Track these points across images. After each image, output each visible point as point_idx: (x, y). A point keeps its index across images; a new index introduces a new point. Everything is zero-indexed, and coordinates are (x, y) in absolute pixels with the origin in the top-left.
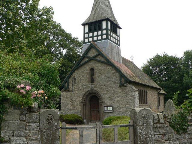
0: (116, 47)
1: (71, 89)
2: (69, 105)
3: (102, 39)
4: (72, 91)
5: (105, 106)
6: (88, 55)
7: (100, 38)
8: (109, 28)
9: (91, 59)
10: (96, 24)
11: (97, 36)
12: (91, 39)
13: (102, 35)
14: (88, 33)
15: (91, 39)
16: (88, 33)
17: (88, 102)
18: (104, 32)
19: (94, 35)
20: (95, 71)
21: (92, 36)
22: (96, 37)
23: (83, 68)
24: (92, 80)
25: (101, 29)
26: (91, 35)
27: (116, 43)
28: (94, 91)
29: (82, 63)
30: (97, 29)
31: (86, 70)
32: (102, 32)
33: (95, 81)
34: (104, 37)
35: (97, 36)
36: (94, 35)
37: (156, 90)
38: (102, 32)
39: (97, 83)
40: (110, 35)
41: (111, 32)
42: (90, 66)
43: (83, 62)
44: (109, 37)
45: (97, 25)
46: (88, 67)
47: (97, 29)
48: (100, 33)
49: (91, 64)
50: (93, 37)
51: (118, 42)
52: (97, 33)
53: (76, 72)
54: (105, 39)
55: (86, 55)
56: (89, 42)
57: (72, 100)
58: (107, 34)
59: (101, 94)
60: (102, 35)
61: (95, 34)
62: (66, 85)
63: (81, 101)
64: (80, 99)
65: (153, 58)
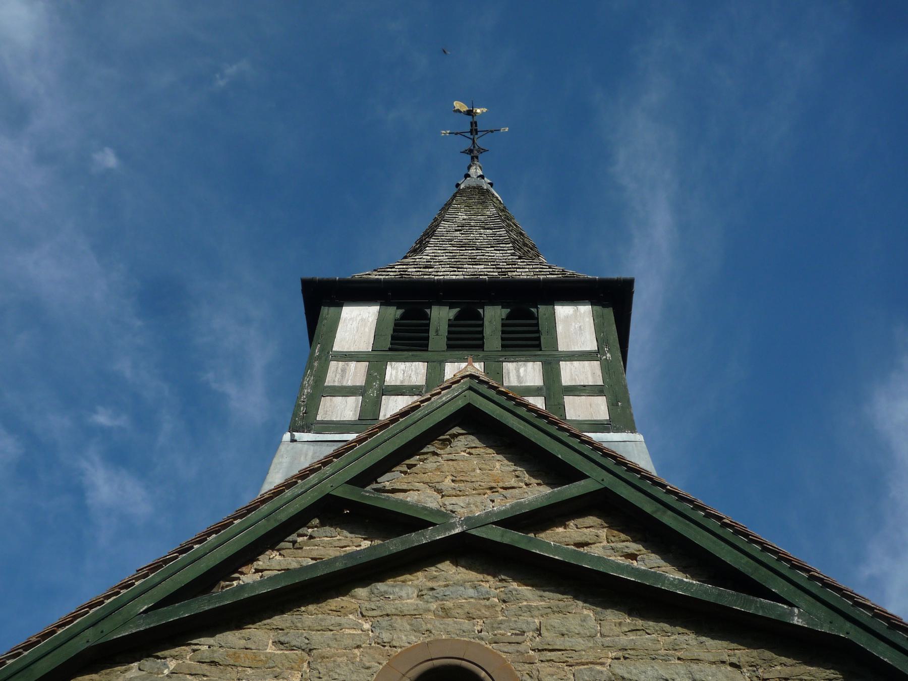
23: (261, 637)
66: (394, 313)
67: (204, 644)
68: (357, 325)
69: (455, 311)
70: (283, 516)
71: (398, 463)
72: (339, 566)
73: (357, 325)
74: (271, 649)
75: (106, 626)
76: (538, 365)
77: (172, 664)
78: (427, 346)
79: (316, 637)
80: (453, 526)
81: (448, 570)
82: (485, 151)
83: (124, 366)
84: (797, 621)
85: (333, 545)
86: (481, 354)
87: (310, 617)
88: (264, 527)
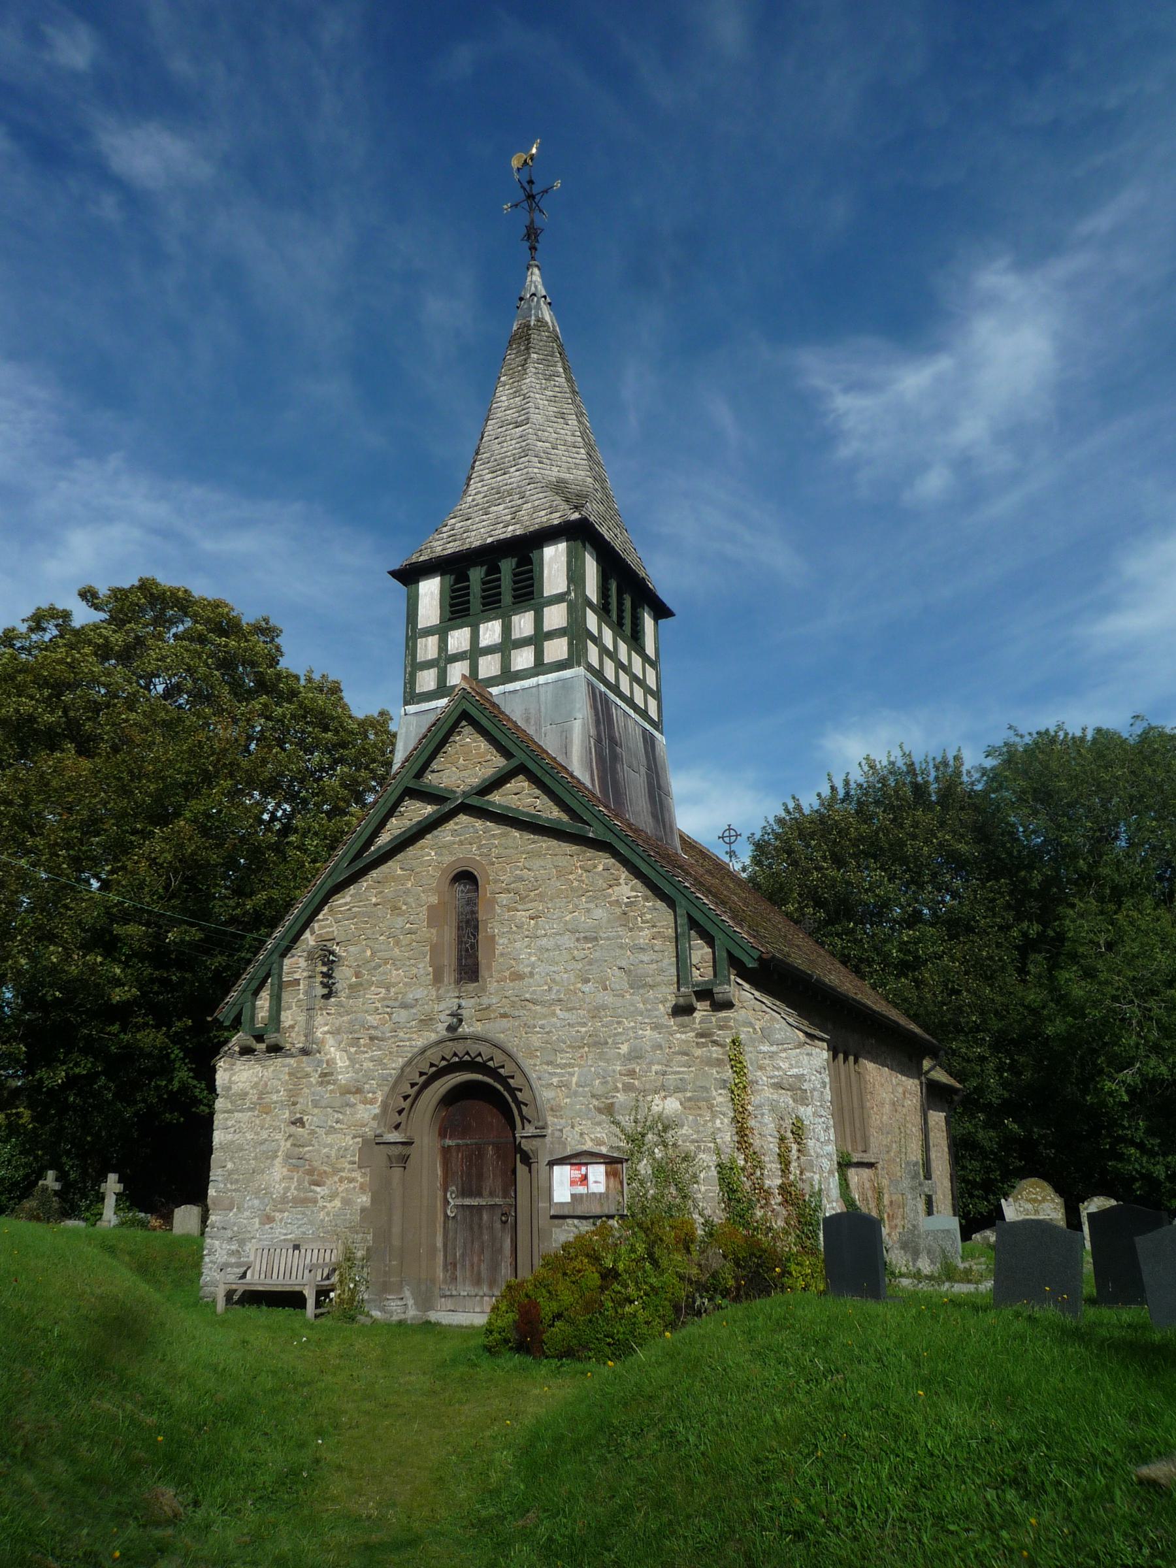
0: (638, 731)
1: (295, 1040)
2: (278, 1171)
3: (540, 667)
4: (305, 1052)
5: (552, 1164)
6: (430, 778)
7: (523, 659)
8: (592, 591)
9: (451, 807)
10: (494, 569)
11: (507, 645)
12: (457, 673)
13: (539, 638)
14: (441, 631)
15: (457, 673)
16: (441, 631)
17: (427, 1144)
18: (556, 616)
19: (547, 627)
20: (487, 889)
21: (465, 646)
22: (498, 656)
23: (393, 867)
24: (469, 968)
25: (528, 593)
26: (459, 639)
27: (635, 707)
28: (474, 1048)
29: (384, 838)
30: (507, 598)
31: (411, 885)
32: (539, 621)
33: (483, 972)
34: (557, 649)
35: (507, 645)
36: (547, 627)
37: (911, 1060)
38: (539, 621)
39: (495, 988)
40: (597, 641)
41: (601, 619)
42: (448, 859)
43: (396, 827)
44: (593, 652)
45: (507, 566)
46: (433, 857)
47: (507, 598)
48: (523, 624)
49: (462, 839)
50: (475, 653)
51: (651, 700)
52: (507, 630)
53: (343, 900)
54: (561, 666)
55: (420, 774)
56: (442, 689)
57: (299, 1122)
58: (576, 633)
59: (513, 1044)
60: (539, 638)
61: (491, 632)
62: (264, 1002)
63: (370, 1134)
64: (367, 1113)
65: (119, 594)
66: (450, 579)
67: (374, 874)
68: (430, 589)
69: (485, 568)
70: (389, 805)
71: (438, 753)
72: (415, 830)
73: (430, 589)
74: (399, 872)
75: (334, 877)
76: (532, 612)
77: (365, 884)
78: (468, 609)
79: (414, 863)
80: (457, 799)
81: (463, 818)
82: (533, 248)
83: (170, 1531)
84: (591, 835)
85: (417, 811)
86: (499, 611)
87: (411, 851)
88: (385, 810)
